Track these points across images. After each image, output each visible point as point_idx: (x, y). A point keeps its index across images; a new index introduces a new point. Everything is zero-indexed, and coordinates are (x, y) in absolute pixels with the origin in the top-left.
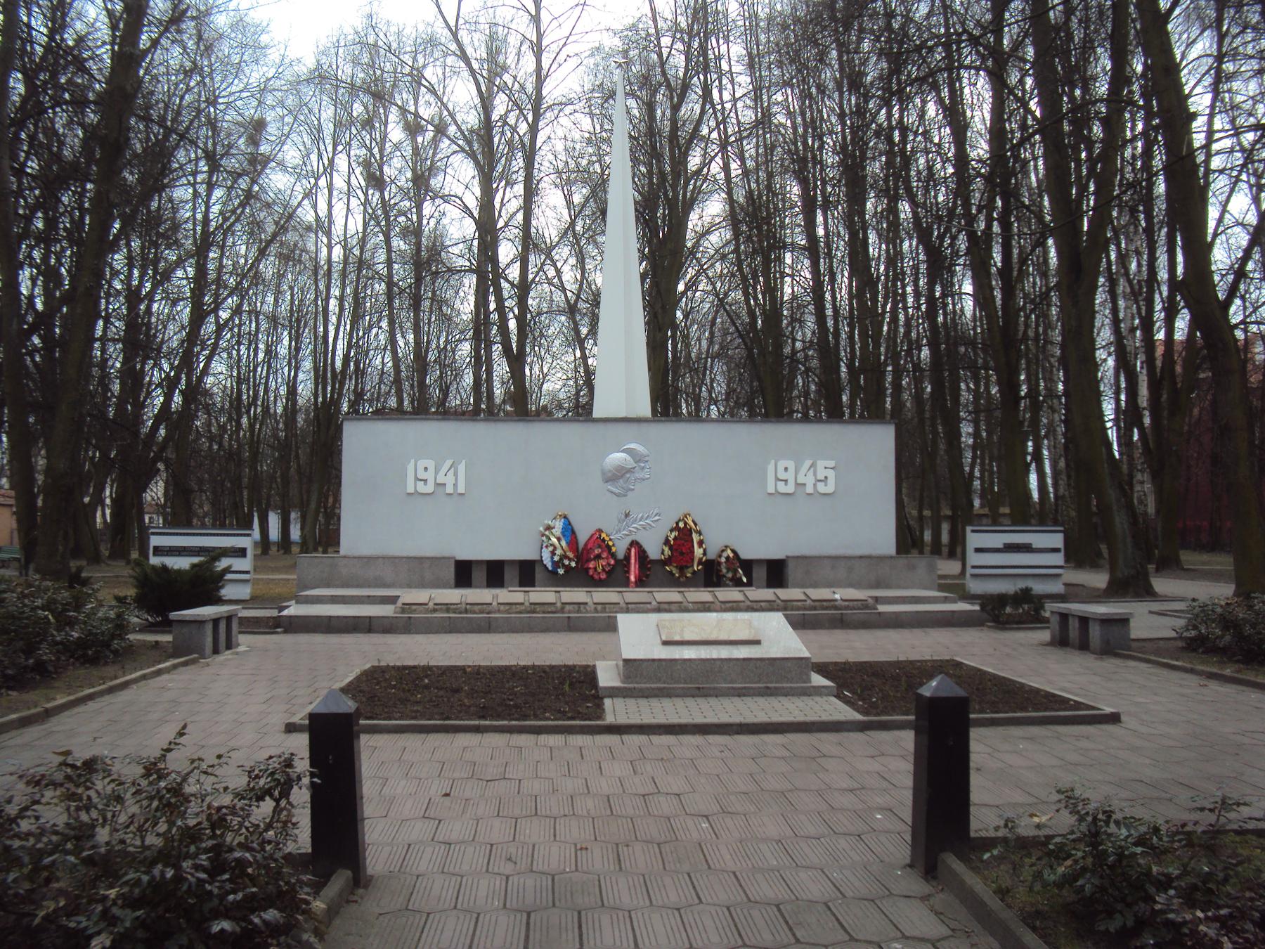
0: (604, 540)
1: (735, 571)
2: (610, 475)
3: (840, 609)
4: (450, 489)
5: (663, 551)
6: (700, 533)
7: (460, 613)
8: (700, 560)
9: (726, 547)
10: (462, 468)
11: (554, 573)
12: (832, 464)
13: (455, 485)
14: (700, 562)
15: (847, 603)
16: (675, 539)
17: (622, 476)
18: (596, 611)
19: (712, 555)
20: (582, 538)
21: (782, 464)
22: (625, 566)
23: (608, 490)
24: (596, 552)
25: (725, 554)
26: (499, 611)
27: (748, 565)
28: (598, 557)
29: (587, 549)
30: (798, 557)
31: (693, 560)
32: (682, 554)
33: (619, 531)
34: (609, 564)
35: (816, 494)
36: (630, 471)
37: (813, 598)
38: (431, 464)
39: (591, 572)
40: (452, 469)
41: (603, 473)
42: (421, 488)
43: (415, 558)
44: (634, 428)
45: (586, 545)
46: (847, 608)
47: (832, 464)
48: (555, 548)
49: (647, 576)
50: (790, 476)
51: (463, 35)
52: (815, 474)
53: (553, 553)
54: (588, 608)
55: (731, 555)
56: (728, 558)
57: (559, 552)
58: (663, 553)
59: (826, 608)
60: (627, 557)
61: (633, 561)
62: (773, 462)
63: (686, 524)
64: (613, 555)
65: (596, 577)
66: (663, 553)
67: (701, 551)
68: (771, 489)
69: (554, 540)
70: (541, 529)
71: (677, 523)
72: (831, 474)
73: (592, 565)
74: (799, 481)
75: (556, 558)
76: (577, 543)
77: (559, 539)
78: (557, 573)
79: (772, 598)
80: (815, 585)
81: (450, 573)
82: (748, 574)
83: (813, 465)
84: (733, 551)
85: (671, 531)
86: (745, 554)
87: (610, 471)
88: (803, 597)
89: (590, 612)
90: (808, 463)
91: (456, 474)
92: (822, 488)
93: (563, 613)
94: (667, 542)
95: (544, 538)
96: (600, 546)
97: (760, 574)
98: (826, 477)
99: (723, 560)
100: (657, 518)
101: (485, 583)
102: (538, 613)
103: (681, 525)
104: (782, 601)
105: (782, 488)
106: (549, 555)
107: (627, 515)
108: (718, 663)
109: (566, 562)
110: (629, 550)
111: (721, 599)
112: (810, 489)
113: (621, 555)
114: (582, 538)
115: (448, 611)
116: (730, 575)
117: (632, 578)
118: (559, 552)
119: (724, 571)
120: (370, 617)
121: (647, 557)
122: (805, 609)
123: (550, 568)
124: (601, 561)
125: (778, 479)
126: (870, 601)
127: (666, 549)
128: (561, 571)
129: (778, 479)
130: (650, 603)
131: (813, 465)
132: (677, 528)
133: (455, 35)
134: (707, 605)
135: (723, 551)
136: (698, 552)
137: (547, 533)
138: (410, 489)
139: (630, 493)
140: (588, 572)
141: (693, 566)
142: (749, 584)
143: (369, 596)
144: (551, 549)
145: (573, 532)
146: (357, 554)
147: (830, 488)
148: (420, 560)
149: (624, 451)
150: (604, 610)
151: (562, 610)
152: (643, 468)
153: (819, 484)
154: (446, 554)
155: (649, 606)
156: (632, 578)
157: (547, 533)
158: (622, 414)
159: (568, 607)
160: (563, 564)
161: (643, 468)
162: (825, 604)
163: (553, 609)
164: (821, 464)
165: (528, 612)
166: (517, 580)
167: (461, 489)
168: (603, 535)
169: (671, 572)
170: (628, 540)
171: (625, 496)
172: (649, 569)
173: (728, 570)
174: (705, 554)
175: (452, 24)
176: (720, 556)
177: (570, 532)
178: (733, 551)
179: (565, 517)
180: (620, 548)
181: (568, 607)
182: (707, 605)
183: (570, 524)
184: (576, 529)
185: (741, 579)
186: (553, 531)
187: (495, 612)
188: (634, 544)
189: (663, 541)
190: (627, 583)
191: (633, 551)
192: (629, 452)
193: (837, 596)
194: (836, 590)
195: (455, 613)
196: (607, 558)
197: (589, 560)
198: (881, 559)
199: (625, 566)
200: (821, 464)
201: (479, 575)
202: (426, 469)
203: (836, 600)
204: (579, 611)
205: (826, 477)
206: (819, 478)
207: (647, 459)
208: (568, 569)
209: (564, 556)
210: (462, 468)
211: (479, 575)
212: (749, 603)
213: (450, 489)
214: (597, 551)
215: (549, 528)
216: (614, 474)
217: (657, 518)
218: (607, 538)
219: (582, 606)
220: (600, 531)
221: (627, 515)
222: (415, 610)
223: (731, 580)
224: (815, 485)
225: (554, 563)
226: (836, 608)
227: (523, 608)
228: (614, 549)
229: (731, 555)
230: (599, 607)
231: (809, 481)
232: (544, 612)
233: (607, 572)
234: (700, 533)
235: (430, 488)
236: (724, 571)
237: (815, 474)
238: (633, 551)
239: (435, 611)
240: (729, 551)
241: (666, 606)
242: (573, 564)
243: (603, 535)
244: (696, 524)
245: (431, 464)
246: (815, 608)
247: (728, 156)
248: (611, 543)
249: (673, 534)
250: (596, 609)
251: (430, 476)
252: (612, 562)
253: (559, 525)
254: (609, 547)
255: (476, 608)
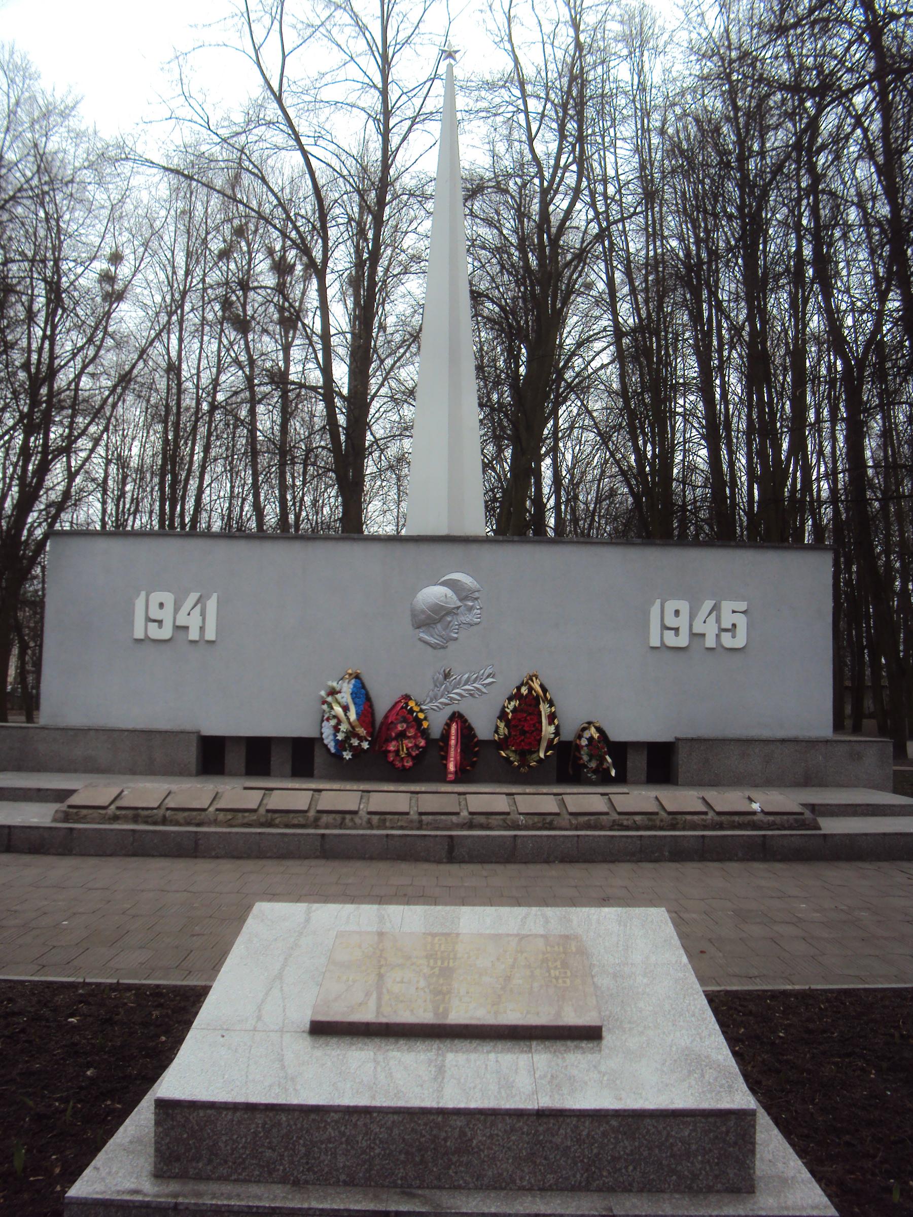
0: (411, 711)
1: (602, 760)
2: (423, 617)
3: (761, 829)
4: (194, 635)
5: (497, 727)
6: (551, 703)
7: (155, 823)
8: (550, 741)
9: (589, 723)
10: (212, 605)
11: (338, 756)
12: (743, 606)
13: (202, 629)
14: (550, 746)
15: (771, 818)
16: (514, 711)
17: (440, 620)
18: (370, 825)
19: (568, 734)
20: (382, 706)
21: (671, 606)
22: (442, 749)
23: (421, 640)
24: (400, 728)
25: (587, 734)
26: (215, 822)
27: (620, 750)
28: (402, 735)
29: (387, 724)
30: (692, 740)
31: (539, 741)
32: (523, 733)
33: (435, 698)
34: (416, 746)
35: (720, 649)
36: (452, 612)
37: (718, 809)
38: (168, 598)
39: (391, 757)
40: (199, 606)
41: (414, 614)
42: (155, 632)
43: (142, 731)
44: (458, 551)
45: (386, 717)
46: (771, 826)
47: (743, 606)
48: (339, 722)
49: (473, 764)
50: (682, 622)
51: (287, 101)
52: (718, 620)
53: (336, 729)
54: (358, 821)
55: (596, 736)
56: (591, 739)
57: (344, 727)
58: (496, 731)
59: (740, 826)
60: (446, 736)
61: (453, 742)
62: (658, 602)
63: (531, 689)
64: (425, 733)
65: (398, 764)
66: (496, 731)
67: (552, 729)
68: (655, 642)
69: (338, 710)
70: (323, 693)
71: (519, 688)
72: (741, 621)
73: (392, 747)
74: (695, 631)
75: (340, 737)
76: (372, 714)
77: (346, 709)
78: (341, 758)
79: (652, 807)
80: (714, 783)
81: (191, 755)
82: (621, 763)
83: (716, 608)
84: (599, 729)
85: (510, 699)
86: (617, 735)
87: (423, 612)
88: (702, 808)
89: (360, 827)
90: (708, 604)
91: (203, 614)
92: (727, 640)
93: (317, 827)
94: (503, 715)
95: (325, 707)
96: (405, 720)
97: (637, 763)
98: (734, 625)
99: (584, 742)
100: (490, 680)
101: (243, 769)
102: (277, 826)
103: (524, 691)
104: (670, 813)
105: (671, 639)
106: (331, 731)
107: (447, 676)
108: (460, 1122)
109: (355, 742)
110: (448, 725)
111: (572, 809)
112: (710, 642)
113: (436, 733)
114: (382, 706)
115: (136, 819)
116: (593, 765)
117: (451, 767)
118: (344, 727)
119: (585, 758)
120: (9, 827)
121: (475, 736)
122: (705, 827)
123: (333, 750)
124: (405, 742)
125: (665, 628)
126: (808, 814)
127: (502, 725)
128: (347, 755)
129: (665, 628)
130: (457, 814)
131: (716, 608)
132: (517, 696)
133: (279, 99)
134: (549, 818)
135: (584, 729)
136: (548, 730)
137: (329, 699)
138: (139, 634)
139: (452, 646)
140: (386, 757)
141: (538, 751)
142: (621, 779)
143: (39, 790)
144: (333, 722)
145: (368, 699)
146: (62, 724)
147: (740, 641)
148: (149, 734)
149: (444, 584)
150: (382, 825)
151: (315, 824)
152: (470, 609)
153: (723, 634)
154: (189, 727)
155: (454, 819)
156: (451, 767)
157: (329, 699)
158: (443, 531)
159: (325, 819)
160: (351, 745)
161: (470, 609)
162: (736, 818)
163: (301, 820)
164: (727, 606)
165: (262, 825)
166: (288, 768)
167: (210, 635)
168: (412, 704)
169: (507, 759)
170: (448, 711)
171: (443, 648)
172: (476, 754)
173: (591, 757)
174: (557, 733)
175: (276, 88)
176: (580, 737)
177: (362, 695)
178: (599, 729)
179: (357, 677)
180: (436, 723)
181: (325, 819)
182: (549, 818)
183: (363, 687)
184: (373, 694)
185: (608, 771)
186: (339, 696)
187: (209, 824)
188: (457, 717)
189: (497, 714)
190: (440, 776)
191: (454, 727)
192: (452, 585)
193: (756, 807)
194: (754, 794)
195: (147, 823)
196: (415, 737)
197: (388, 740)
198: (813, 743)
199: (442, 749)
200: (727, 606)
201: (235, 758)
202: (161, 605)
203: (754, 813)
204: (342, 826)
205: (734, 625)
206: (724, 626)
207: (476, 595)
208: (357, 751)
209: (352, 733)
210: (212, 605)
211: (235, 758)
212: (616, 817)
213: (194, 635)
214: (400, 727)
215: (333, 692)
216: (429, 617)
217: (490, 680)
218: (416, 709)
219: (348, 817)
220: (407, 698)
221: (447, 676)
222: (85, 816)
223: (595, 771)
224: (718, 636)
225: (337, 742)
226: (755, 826)
227: (254, 817)
228: (425, 724)
229: (596, 736)
230: (375, 819)
231: (710, 630)
232: (287, 826)
233: (413, 758)
234: (551, 703)
235: (166, 633)
236: (585, 758)
237: (718, 620)
238: (454, 727)
239: (115, 818)
240: (593, 730)
241: (482, 819)
242: (365, 745)
243: (412, 704)
244: (545, 690)
245: (168, 598)
246: (720, 826)
247: (612, 267)
248: (421, 716)
249: (513, 703)
250: (369, 822)
251: (166, 615)
252: (422, 743)
253: (347, 689)
254: (419, 722)
255: (181, 816)
